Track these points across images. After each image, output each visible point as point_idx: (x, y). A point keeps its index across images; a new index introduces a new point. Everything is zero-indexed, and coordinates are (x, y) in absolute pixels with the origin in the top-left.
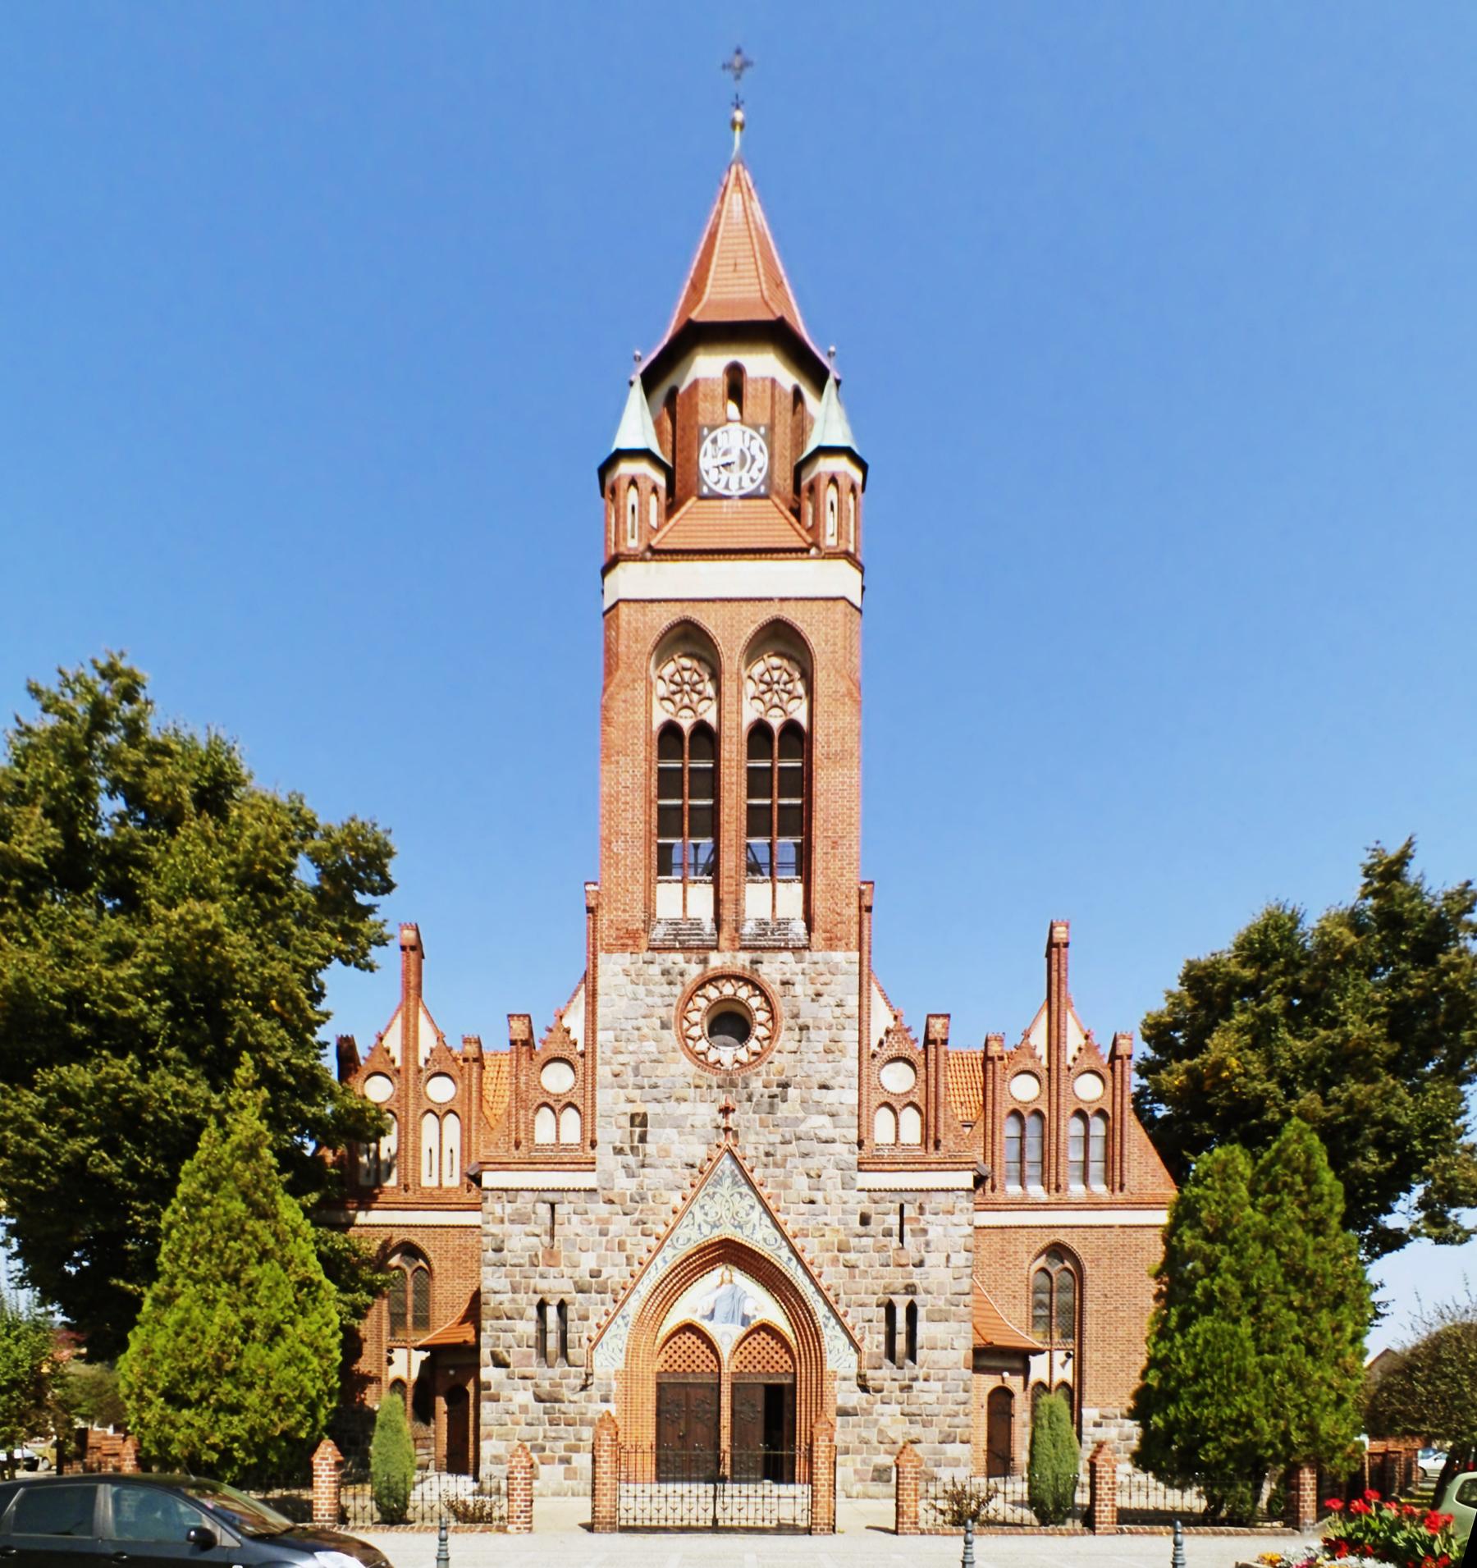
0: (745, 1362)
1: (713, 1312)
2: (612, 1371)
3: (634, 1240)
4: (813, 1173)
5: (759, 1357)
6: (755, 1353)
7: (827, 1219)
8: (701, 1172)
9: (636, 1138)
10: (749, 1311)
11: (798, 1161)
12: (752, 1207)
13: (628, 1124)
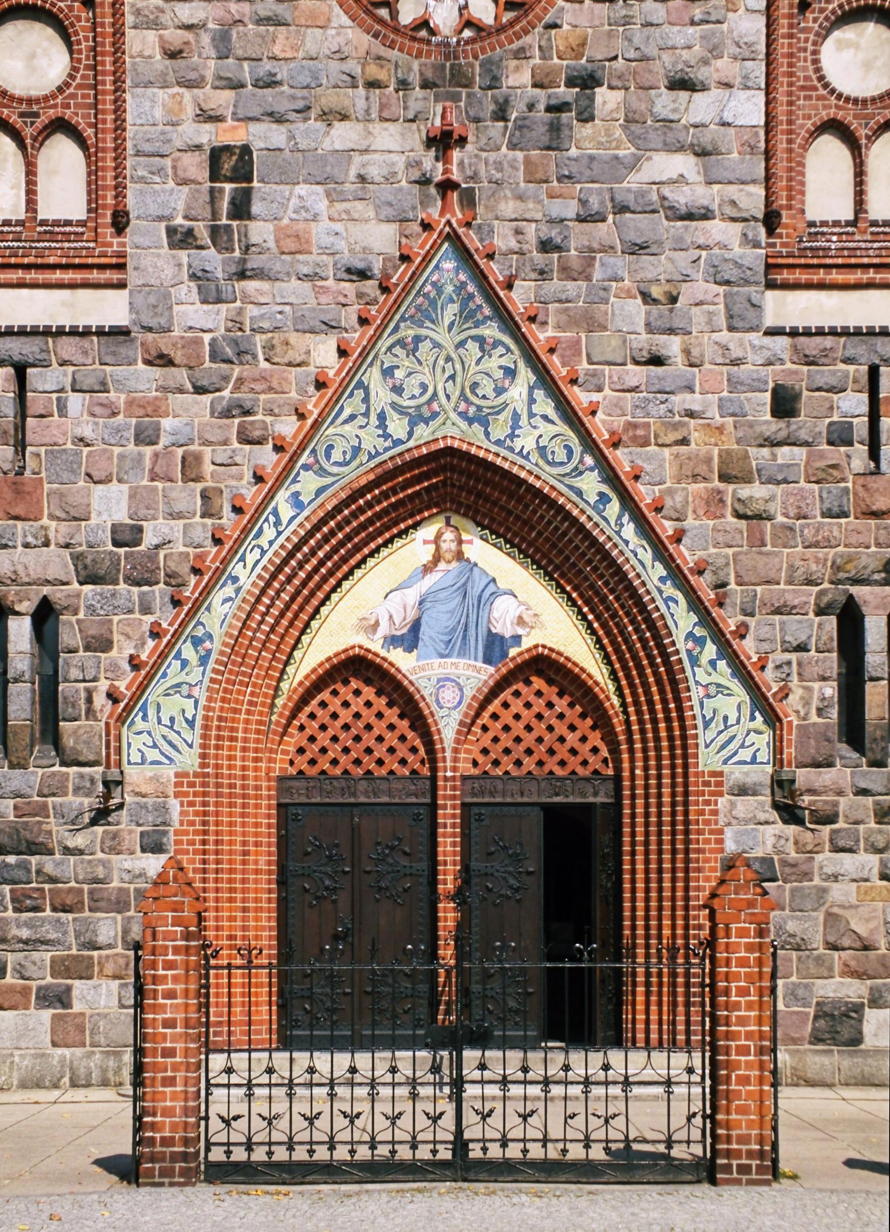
1: (416, 626)
2: (168, 773)
4: (656, 292)
5: (529, 739)
6: (518, 728)
7: (694, 401)
10: (504, 627)
11: (620, 263)
12: (511, 373)
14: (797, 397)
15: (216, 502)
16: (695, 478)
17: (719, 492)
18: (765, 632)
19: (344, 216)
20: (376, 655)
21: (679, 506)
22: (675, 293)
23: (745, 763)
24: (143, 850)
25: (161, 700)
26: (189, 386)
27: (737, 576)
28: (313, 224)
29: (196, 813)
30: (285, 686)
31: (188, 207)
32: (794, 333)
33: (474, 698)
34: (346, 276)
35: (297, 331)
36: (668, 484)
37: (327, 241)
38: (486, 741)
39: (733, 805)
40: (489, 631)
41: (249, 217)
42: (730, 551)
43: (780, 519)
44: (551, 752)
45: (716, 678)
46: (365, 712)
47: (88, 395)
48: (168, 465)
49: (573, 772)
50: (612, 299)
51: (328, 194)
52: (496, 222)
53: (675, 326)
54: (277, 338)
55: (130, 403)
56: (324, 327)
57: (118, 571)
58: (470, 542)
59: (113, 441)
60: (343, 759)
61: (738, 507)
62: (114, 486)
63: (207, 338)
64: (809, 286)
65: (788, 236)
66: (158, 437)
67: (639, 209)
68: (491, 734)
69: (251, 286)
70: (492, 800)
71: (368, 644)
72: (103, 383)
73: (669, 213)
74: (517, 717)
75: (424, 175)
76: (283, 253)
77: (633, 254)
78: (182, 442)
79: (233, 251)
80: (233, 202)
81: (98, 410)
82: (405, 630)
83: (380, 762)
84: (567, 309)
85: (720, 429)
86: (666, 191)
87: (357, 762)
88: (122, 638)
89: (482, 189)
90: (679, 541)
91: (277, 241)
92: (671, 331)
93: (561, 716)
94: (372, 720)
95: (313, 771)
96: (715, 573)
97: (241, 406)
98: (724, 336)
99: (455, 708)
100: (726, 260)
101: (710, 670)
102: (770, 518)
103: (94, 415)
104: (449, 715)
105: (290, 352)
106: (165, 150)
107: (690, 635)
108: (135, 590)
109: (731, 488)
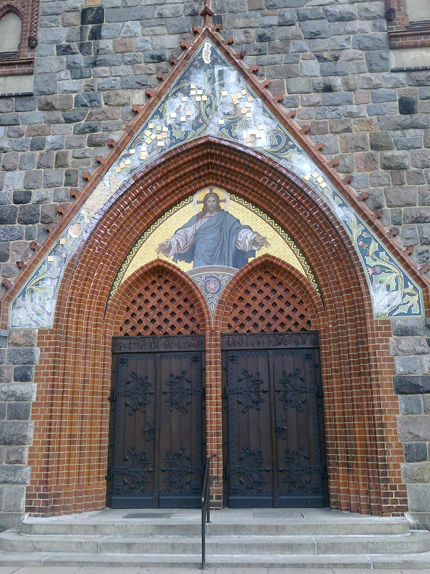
0: (242, 319)
1: (193, 248)
3: (78, 153)
4: (325, 55)
5: (262, 311)
6: (255, 305)
7: (354, 108)
8: (173, 64)
9: (88, 33)
11: (304, 44)
13: (78, 21)
14: (414, 102)
15: (73, 178)
16: (357, 148)
17: (372, 155)
18: (408, 233)
19: (151, 33)
20: (170, 264)
21: (348, 164)
22: (337, 55)
23: (403, 314)
24: (16, 380)
25: (34, 287)
26: (62, 119)
27: (388, 201)
28: (134, 38)
29: (50, 356)
30: (116, 284)
31: (69, 36)
32: (409, 71)
33: (228, 287)
34: (151, 60)
35: (123, 88)
36: (340, 153)
37: (140, 44)
38: (236, 313)
39: (399, 342)
40: (236, 248)
41: (100, 38)
42: (382, 188)
43: (412, 169)
44: (275, 318)
45: (379, 263)
46: (164, 299)
47: (7, 127)
48: (48, 159)
49: (290, 330)
50: (301, 61)
51: (142, 25)
52: (233, 30)
53: (338, 71)
54: (111, 93)
55: (29, 130)
56: (138, 85)
57: (16, 216)
58: (224, 201)
59: (18, 149)
60: (151, 326)
61: (384, 162)
62: (17, 172)
63: (74, 95)
64: (415, 46)
65: (400, 23)
66: (44, 145)
67: (314, 17)
68: (239, 309)
69: (99, 69)
70: (240, 348)
71: (164, 258)
72: (16, 120)
73: (330, 18)
74: (254, 298)
75: (194, 10)
76: (118, 53)
77: (311, 39)
78: (57, 147)
79: (91, 54)
80: (92, 32)
81: (12, 134)
82: (186, 250)
83: (173, 327)
84: (275, 67)
85: (370, 122)
86: (328, 8)
87: (159, 327)
88: (14, 253)
89: (226, 17)
90: (349, 183)
91: (114, 47)
92: (336, 74)
93: (281, 297)
94: (169, 303)
95: (133, 334)
96: (374, 200)
97: (90, 127)
98: (368, 75)
99: (216, 293)
100: (365, 37)
101: (375, 257)
102: (405, 168)
103: (10, 137)
104: (212, 297)
105: (119, 99)
106: (59, 11)
107: (360, 237)
108: (24, 226)
109: (379, 153)
